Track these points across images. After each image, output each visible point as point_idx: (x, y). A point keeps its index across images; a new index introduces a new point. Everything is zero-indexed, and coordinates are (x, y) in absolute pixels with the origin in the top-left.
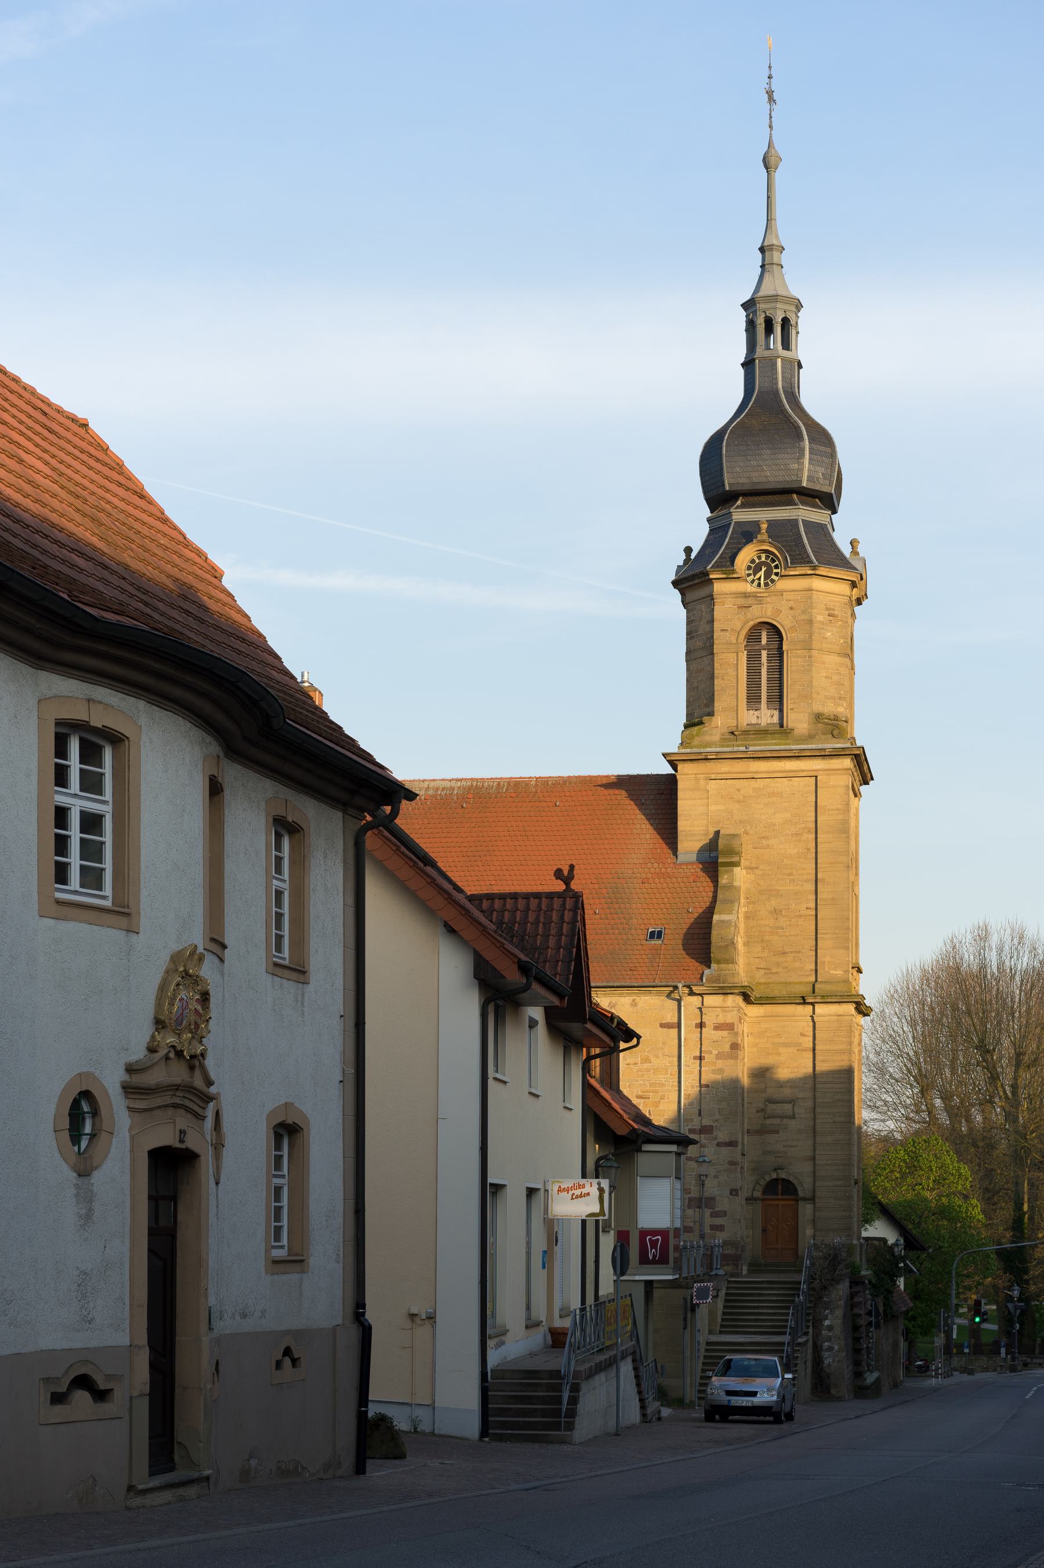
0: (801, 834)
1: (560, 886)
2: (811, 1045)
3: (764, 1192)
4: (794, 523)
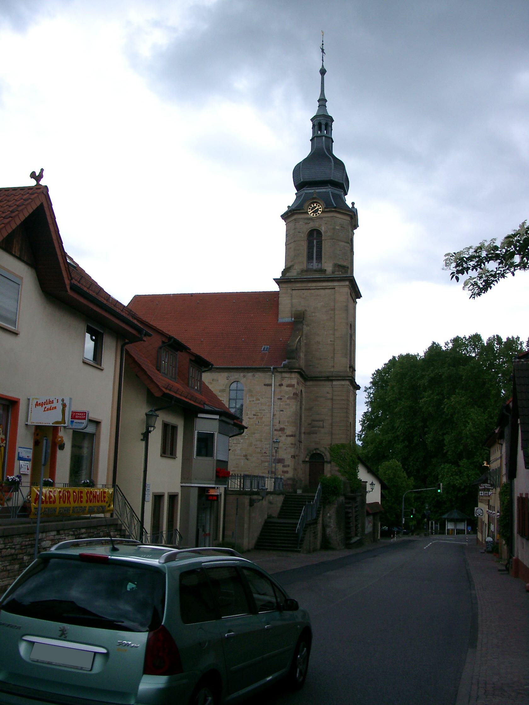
1: (33, 183)
3: (310, 459)
4: (327, 193)
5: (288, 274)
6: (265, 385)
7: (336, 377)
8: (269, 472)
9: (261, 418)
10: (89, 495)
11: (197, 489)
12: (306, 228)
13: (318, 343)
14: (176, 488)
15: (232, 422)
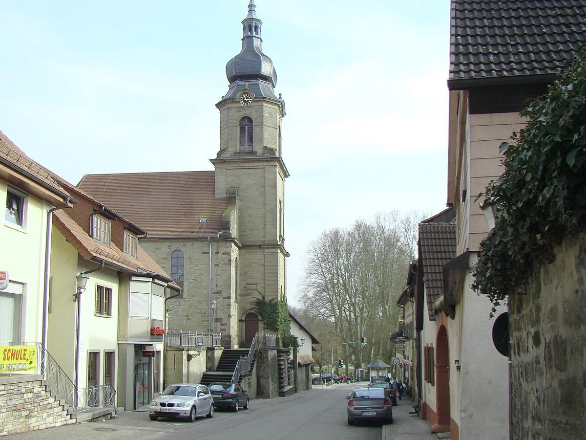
5: (222, 156)
6: (203, 253)
7: (267, 245)
8: (208, 330)
9: (200, 283)
10: (6, 353)
11: (133, 345)
12: (238, 116)
13: (251, 215)
14: (113, 347)
15: (166, 284)
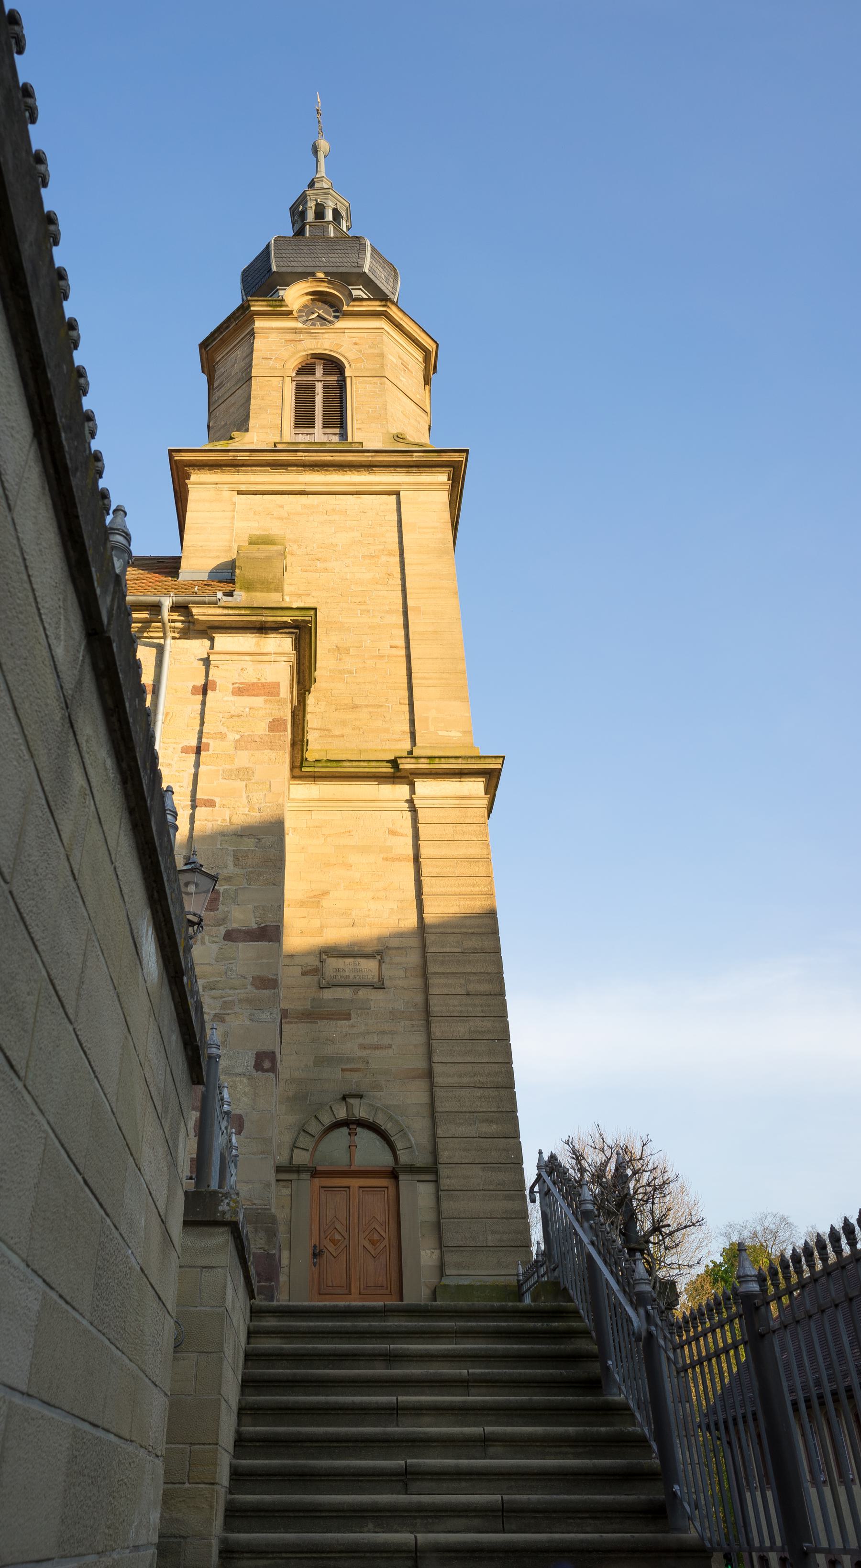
0: (378, 557)
2: (410, 851)
